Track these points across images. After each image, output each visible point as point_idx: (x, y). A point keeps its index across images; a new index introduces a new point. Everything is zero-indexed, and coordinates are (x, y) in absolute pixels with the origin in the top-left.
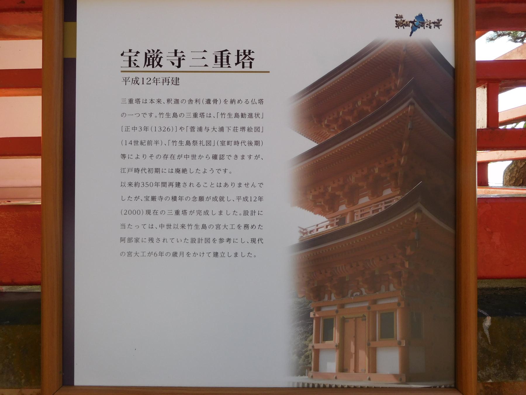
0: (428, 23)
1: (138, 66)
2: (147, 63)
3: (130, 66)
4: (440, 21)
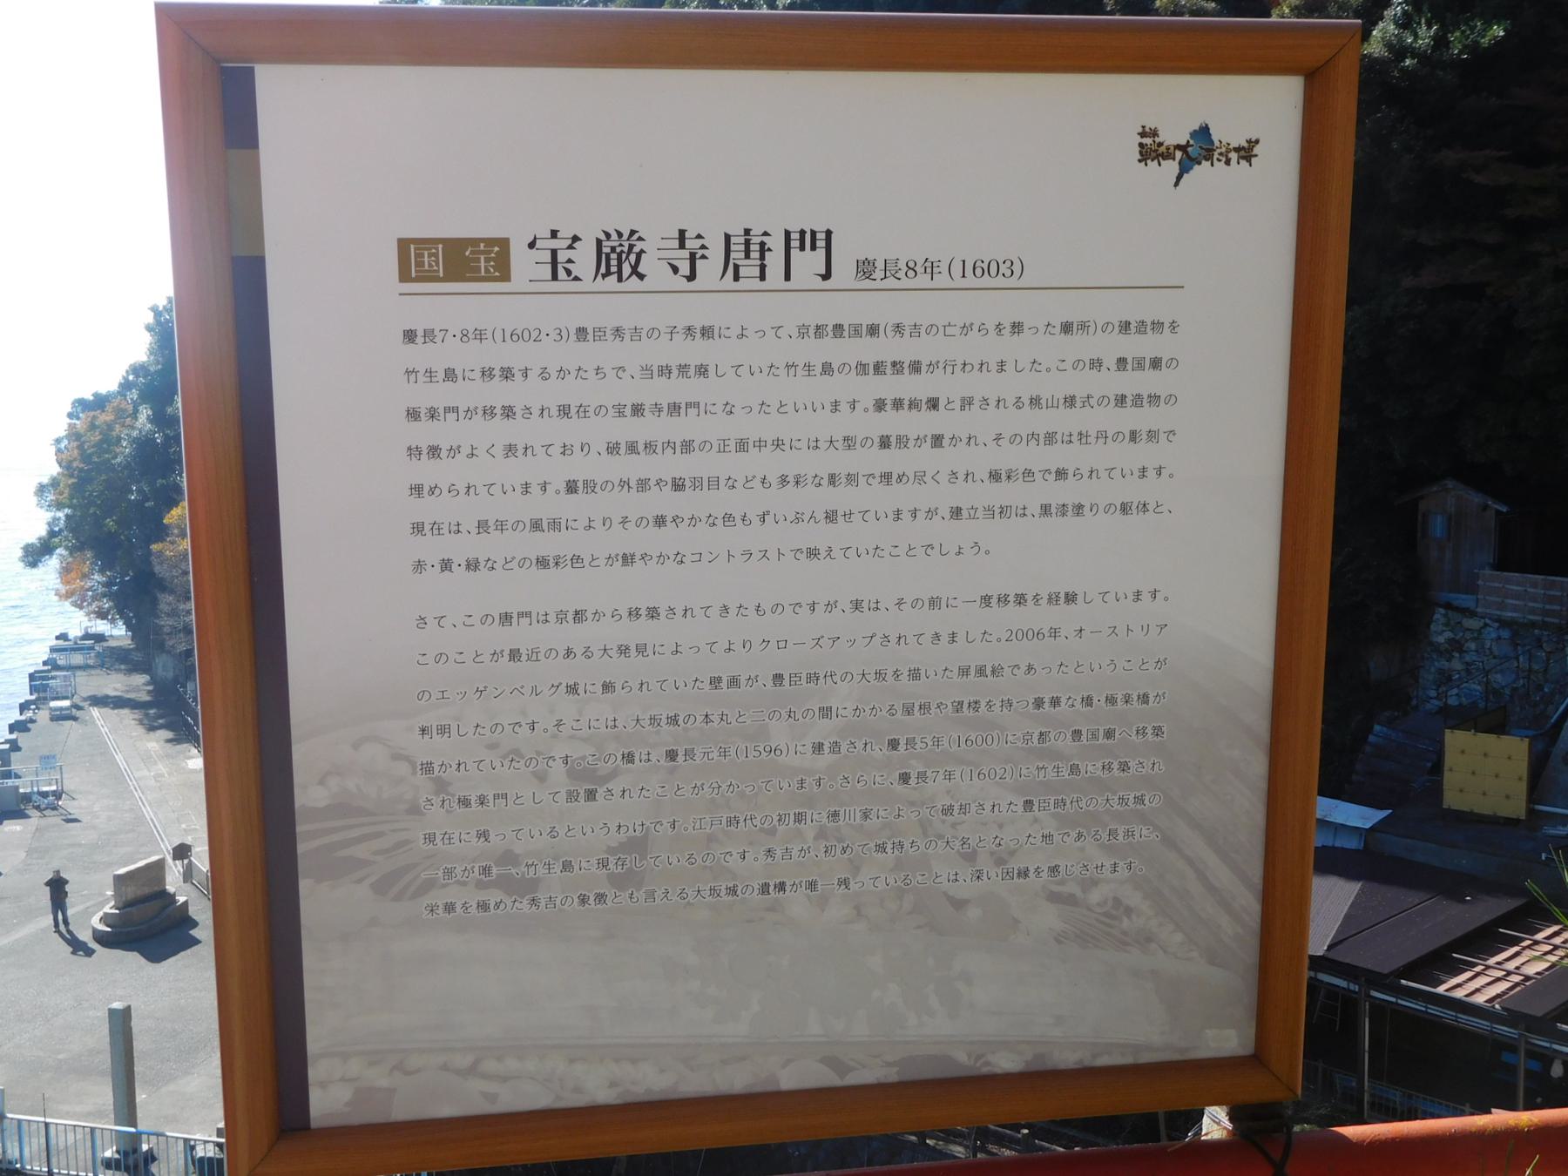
1: (576, 279)
2: (603, 270)
3: (555, 277)
4: (1253, 143)
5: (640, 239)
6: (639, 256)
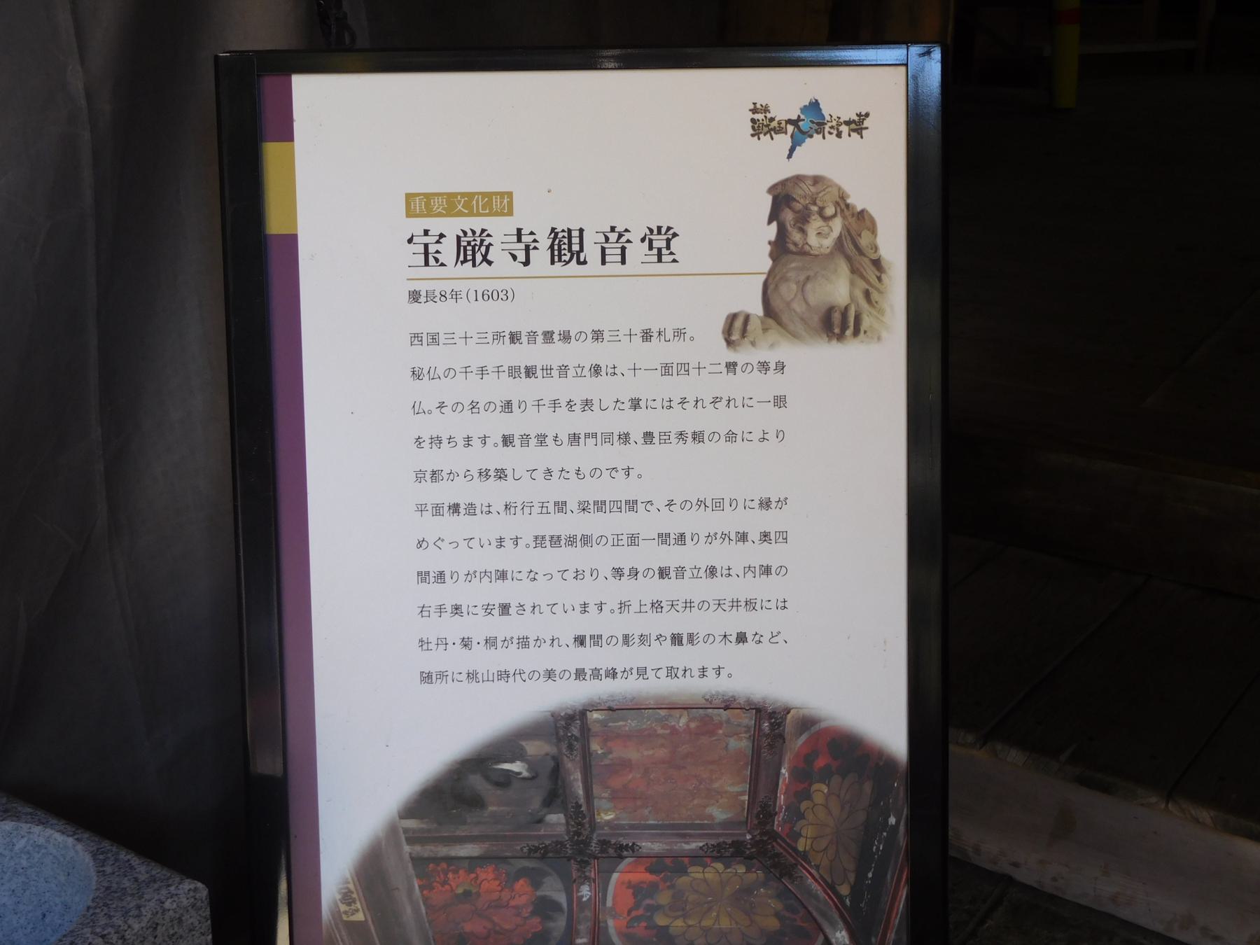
0: (834, 123)
1: (443, 265)
2: (462, 258)
3: (427, 264)
4: (863, 116)
5: (489, 235)
6: (488, 248)
